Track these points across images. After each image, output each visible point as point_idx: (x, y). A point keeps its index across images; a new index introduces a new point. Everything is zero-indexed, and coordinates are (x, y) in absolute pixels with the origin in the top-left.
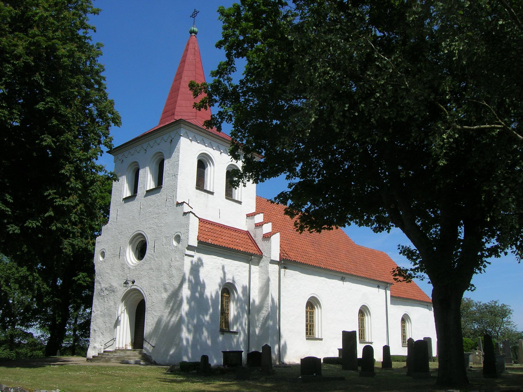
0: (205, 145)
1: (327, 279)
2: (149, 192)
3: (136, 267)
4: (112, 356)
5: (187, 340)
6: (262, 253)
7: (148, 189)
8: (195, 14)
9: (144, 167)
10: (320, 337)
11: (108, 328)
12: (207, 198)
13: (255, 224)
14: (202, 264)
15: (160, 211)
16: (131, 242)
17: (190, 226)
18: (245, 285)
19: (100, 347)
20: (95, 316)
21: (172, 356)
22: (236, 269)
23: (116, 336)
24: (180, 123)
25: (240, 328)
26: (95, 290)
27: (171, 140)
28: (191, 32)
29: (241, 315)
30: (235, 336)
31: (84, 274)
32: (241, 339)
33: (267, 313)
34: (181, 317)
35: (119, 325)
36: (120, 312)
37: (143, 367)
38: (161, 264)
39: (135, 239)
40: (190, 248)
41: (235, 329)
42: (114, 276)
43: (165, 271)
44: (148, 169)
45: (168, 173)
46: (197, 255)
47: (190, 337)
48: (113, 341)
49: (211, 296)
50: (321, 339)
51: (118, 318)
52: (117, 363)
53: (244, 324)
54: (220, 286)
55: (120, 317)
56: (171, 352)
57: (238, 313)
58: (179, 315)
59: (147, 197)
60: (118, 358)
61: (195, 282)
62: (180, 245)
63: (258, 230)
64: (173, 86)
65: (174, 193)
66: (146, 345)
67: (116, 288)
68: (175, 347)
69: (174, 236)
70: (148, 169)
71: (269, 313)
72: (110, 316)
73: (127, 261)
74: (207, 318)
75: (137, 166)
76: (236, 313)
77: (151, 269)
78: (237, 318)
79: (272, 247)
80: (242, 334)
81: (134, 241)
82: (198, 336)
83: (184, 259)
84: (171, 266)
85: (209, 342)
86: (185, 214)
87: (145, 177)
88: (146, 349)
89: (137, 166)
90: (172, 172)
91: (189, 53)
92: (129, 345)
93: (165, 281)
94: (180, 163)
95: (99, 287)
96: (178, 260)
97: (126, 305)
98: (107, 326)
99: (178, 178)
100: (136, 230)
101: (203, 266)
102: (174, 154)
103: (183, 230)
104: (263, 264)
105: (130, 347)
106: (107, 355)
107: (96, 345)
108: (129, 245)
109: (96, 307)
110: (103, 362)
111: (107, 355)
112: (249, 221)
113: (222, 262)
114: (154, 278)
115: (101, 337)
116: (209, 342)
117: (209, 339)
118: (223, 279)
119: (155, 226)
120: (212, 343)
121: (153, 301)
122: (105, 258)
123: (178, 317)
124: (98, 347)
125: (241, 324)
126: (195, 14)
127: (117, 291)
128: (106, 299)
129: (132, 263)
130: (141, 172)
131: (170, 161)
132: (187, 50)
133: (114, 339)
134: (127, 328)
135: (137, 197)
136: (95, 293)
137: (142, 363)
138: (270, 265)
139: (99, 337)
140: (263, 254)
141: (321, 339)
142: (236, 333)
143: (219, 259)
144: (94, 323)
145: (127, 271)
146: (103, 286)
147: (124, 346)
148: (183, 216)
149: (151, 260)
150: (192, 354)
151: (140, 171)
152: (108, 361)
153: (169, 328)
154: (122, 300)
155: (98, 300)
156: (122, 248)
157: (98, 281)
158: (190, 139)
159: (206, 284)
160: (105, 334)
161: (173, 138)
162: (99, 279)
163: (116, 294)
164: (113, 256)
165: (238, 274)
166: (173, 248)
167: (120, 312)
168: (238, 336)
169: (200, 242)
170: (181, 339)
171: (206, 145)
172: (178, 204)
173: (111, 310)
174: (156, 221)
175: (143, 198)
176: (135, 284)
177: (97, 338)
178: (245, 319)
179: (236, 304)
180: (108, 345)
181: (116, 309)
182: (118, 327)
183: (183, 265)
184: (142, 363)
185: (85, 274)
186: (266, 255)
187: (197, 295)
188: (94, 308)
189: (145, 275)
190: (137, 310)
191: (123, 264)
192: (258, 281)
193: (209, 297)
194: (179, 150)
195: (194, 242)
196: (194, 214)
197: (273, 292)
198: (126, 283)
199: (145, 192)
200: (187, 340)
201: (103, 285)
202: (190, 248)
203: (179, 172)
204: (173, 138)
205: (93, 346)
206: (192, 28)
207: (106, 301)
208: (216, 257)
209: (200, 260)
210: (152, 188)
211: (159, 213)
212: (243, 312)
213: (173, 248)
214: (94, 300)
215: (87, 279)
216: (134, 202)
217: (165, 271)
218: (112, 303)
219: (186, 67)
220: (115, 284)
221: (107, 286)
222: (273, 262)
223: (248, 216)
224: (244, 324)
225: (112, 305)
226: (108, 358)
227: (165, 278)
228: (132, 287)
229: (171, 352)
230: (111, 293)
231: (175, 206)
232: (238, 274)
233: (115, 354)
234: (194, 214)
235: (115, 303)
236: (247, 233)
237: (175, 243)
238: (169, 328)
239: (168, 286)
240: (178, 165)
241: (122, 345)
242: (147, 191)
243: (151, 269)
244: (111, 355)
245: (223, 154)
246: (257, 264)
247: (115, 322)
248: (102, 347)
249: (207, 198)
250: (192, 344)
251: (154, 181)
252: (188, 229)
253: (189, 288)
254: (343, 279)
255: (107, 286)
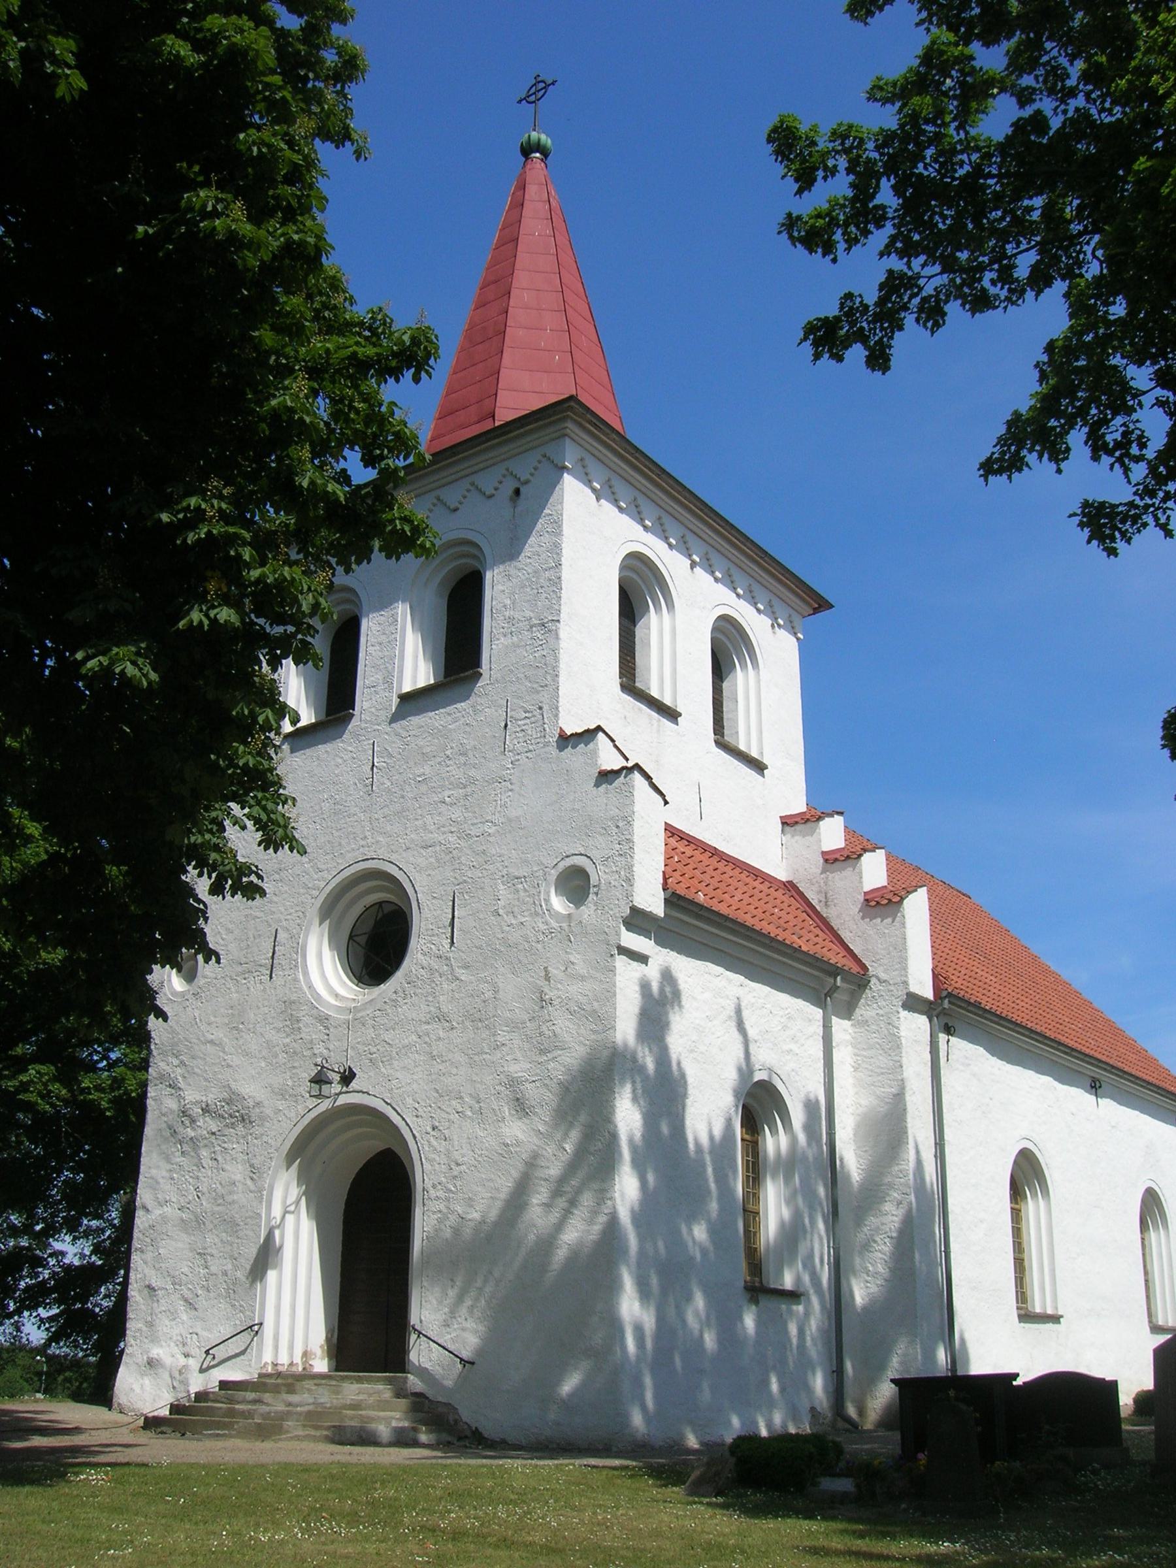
0: (641, 521)
1: (1056, 1084)
2: (412, 702)
3: (355, 1018)
4: (281, 1407)
5: (639, 1330)
6: (864, 968)
7: (407, 688)
8: (538, 90)
9: (384, 603)
10: (1049, 1311)
11: (221, 1279)
12: (658, 731)
13: (824, 853)
14: (677, 994)
15: (472, 773)
16: (327, 911)
17: (637, 824)
18: (812, 1097)
19: (182, 1361)
20: (152, 1227)
21: (569, 1406)
22: (785, 1028)
23: (262, 1314)
24: (564, 419)
25: (806, 1279)
26: (150, 1116)
27: (517, 492)
28: (527, 150)
29: (807, 1221)
30: (790, 1312)
31: (43, 1068)
32: (814, 1324)
33: (901, 1212)
34: (613, 1224)
35: (277, 1265)
36: (277, 1211)
37: (426, 1452)
38: (489, 994)
39: (348, 896)
40: (638, 920)
41: (788, 1281)
42: (247, 1054)
43: (515, 1026)
44: (402, 610)
45: (510, 620)
46: (661, 957)
47: (649, 1321)
48: (246, 1337)
49: (711, 1138)
50: (1055, 1319)
51: (270, 1236)
52: (315, 1439)
53: (817, 1261)
54: (737, 1094)
55: (277, 1232)
56: (569, 1386)
57: (797, 1216)
58: (602, 1219)
59: (404, 723)
60: (313, 1418)
61: (657, 1070)
62: (587, 912)
63: (836, 876)
64: (472, 326)
65: (545, 697)
66: (421, 1354)
67: (258, 1104)
68: (585, 1365)
69: (554, 874)
70: (402, 610)
71: (910, 1210)
72: (232, 1226)
73: (311, 987)
74: (700, 1232)
75: (347, 606)
76: (786, 1213)
77: (442, 1018)
78: (793, 1233)
79: (909, 943)
80: (815, 1300)
81: (340, 906)
82: (671, 1312)
83: (613, 970)
84: (543, 1001)
85: (710, 1340)
86: (606, 776)
87: (393, 643)
88: (422, 1373)
89: (347, 606)
90: (528, 614)
91: (527, 211)
92: (319, 1352)
93: (518, 1069)
94: (566, 573)
95: (172, 1104)
96: (584, 972)
97: (304, 1177)
98: (214, 1269)
99: (562, 634)
100: (350, 857)
101: (680, 1006)
102: (532, 540)
103: (599, 846)
104: (872, 1013)
105: (321, 1365)
106: (255, 1402)
107: (156, 1352)
108: (317, 921)
109: (154, 1186)
110: (245, 1434)
111: (255, 1402)
112: (797, 841)
113: (740, 992)
114: (459, 1057)
115: (184, 1317)
116: (710, 1340)
117: (709, 1326)
118: (746, 1070)
119: (452, 838)
120: (720, 1341)
121: (456, 1155)
122: (200, 981)
123: (597, 1228)
124: (168, 1361)
125: (808, 1263)
126: (538, 90)
127: (263, 1118)
128: (204, 1153)
129: (337, 995)
130: (371, 628)
131: (513, 572)
132: (518, 204)
133: (254, 1329)
134: (309, 1278)
135: (354, 722)
136: (148, 1131)
137: (423, 1438)
138: (904, 1014)
139: (173, 1315)
140: (871, 971)
141: (1055, 1319)
142: (794, 1296)
143: (730, 981)
144: (149, 1256)
145: (311, 1031)
146: (189, 1098)
147: (298, 1359)
148: (597, 785)
149: (437, 979)
150: (656, 1396)
151: (364, 624)
152: (268, 1429)
153: (551, 1276)
154: (290, 1160)
155: (168, 1159)
156: (282, 936)
157: (162, 1077)
158: (594, 490)
159: (690, 1080)
160: (202, 1303)
161: (527, 482)
162: (168, 1069)
163: (257, 1130)
164: (240, 969)
165: (793, 1046)
166: (554, 924)
167: (277, 1211)
168: (800, 1308)
169: (673, 900)
170: (614, 1325)
171: (648, 523)
172: (565, 740)
173: (234, 1202)
174: (457, 814)
175: (385, 727)
176: (354, 1085)
177: (165, 1325)
178: (819, 1244)
179: (788, 1179)
180: (221, 1353)
181: (262, 1195)
182: (271, 1275)
183: (609, 995)
184: (423, 1438)
185: (48, 1069)
186: (883, 976)
187: (665, 1129)
188: (144, 1194)
189: (408, 1047)
190: (348, 1204)
191: (289, 1003)
192: (851, 1080)
193: (705, 1141)
194: (558, 524)
195: (653, 901)
196: (648, 778)
197: (919, 1129)
198: (319, 1080)
199: (395, 701)
200: (639, 1330)
201: (191, 1095)
202: (638, 920)
203: (564, 609)
204: (527, 482)
205: (142, 1359)
206: (534, 135)
207: (207, 1162)
208: (720, 970)
209: (667, 976)
210: (421, 684)
211: (473, 781)
212: (812, 1208)
213: (554, 924)
214: (144, 1160)
215: (55, 1087)
216: (339, 744)
217: (515, 1026)
218: (237, 1172)
219: (523, 258)
220: (251, 1089)
221: (211, 1098)
222: (913, 1003)
223: (788, 822)
224: (817, 1261)
225: (238, 1177)
226: (266, 1416)
227: (519, 1055)
228: (343, 1100)
229: (569, 1386)
230: (233, 1126)
231: (554, 751)
232: (793, 1046)
233: (294, 1398)
234: (648, 778)
235: (255, 1172)
236: (790, 887)
237: (559, 904)
238: (551, 1276)
239: (531, 1092)
240: (557, 582)
241: (291, 1355)
242: (405, 698)
243: (442, 1018)
244: (275, 1404)
245: (698, 570)
246: (847, 1011)
247: (252, 1251)
248: (191, 1361)
249: (658, 731)
250: (658, 1349)
251: (433, 658)
252: (629, 841)
253: (635, 1099)
254: (1095, 1087)
255: (212, 1097)
